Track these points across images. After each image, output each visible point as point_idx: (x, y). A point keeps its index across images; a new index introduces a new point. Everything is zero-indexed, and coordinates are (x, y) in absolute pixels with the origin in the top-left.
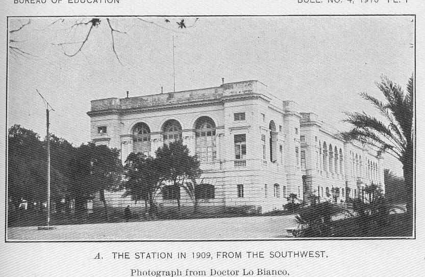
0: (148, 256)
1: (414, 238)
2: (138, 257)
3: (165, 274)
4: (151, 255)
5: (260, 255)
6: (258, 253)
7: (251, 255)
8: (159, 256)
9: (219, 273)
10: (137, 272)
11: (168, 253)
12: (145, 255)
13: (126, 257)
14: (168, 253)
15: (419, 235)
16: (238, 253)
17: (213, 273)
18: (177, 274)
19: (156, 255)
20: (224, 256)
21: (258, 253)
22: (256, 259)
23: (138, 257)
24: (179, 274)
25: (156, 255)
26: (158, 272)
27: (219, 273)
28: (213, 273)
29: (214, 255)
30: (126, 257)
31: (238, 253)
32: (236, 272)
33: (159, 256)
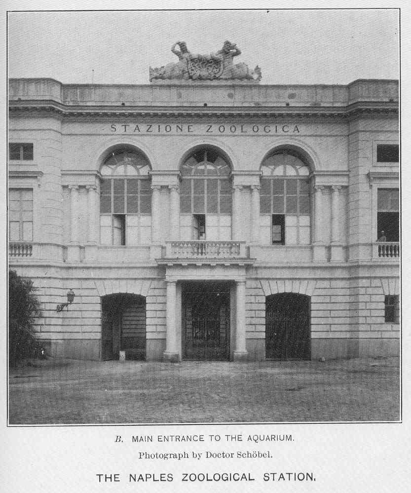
0: (282, 476)
1: (9, 425)
2: (267, 478)
3: (172, 456)
4: (286, 476)
5: (239, 438)
6: (237, 436)
7: (230, 438)
8: (297, 477)
9: (215, 456)
10: (145, 455)
11: (307, 474)
12: (277, 477)
13: (116, 479)
14: (307, 474)
15: (405, 199)
16: (135, 437)
17: (209, 455)
18: (183, 457)
19: (292, 476)
20: (177, 440)
21: (237, 436)
22: (244, 451)
23: (267, 478)
24: (186, 456)
25: (292, 476)
26: (166, 455)
27: (215, 456)
28: (209, 455)
29: (155, 439)
30: (116, 479)
31: (135, 437)
32: (231, 455)
33: (297, 477)
